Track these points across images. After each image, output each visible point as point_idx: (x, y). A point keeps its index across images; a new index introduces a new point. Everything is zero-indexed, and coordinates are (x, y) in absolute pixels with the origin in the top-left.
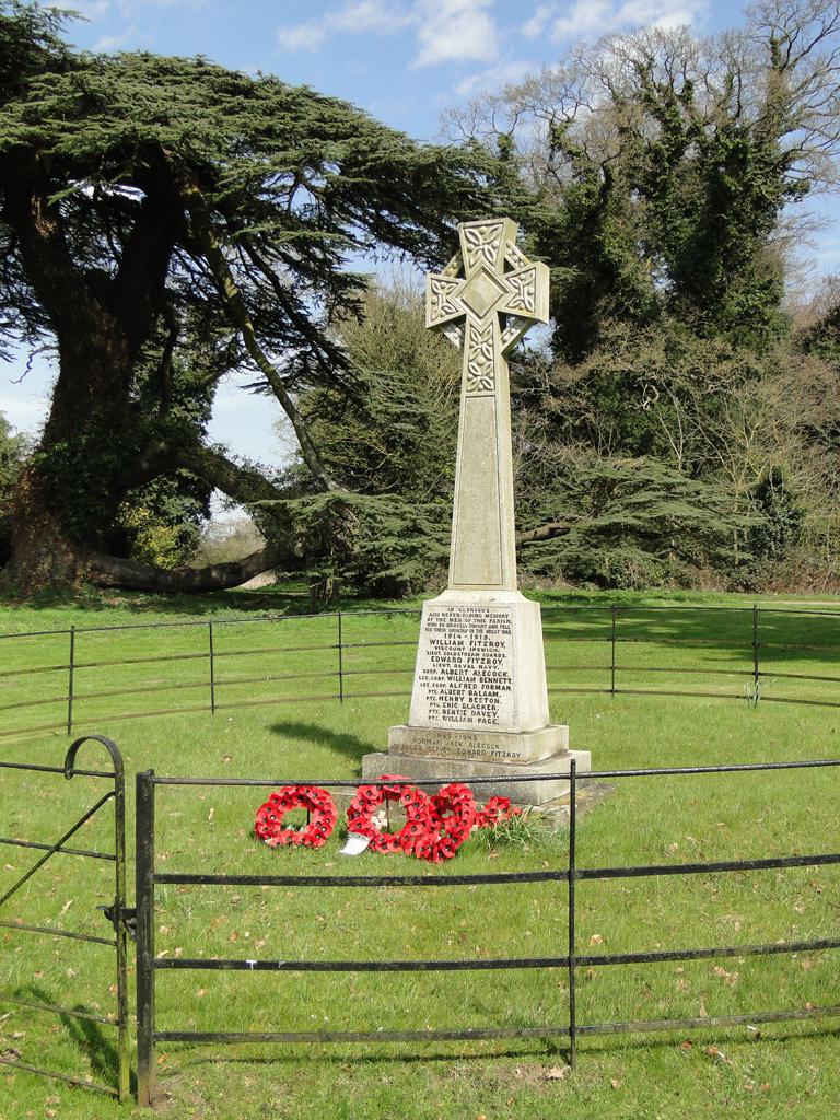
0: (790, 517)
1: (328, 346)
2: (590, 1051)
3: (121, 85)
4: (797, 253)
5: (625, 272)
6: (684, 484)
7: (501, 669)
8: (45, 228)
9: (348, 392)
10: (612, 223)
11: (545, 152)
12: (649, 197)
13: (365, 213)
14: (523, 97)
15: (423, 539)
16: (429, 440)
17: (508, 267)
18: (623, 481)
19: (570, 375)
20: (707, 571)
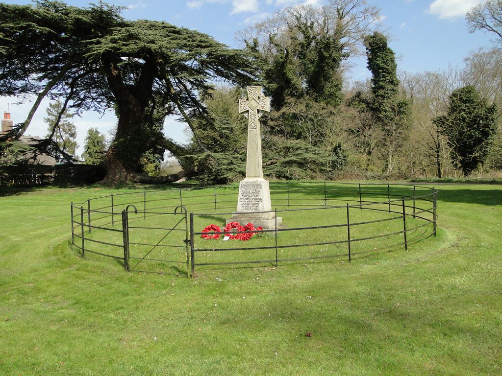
0: (344, 157)
1: (202, 107)
2: (280, 266)
3: (139, 30)
4: (346, 75)
5: (293, 82)
6: (311, 148)
7: (259, 197)
8: (115, 73)
9: (208, 121)
10: (289, 67)
11: (268, 44)
12: (300, 58)
13: (213, 67)
14: (259, 27)
15: (234, 166)
16: (233, 135)
17: (259, 98)
18: (293, 147)
19: (277, 114)
20: (319, 174)
